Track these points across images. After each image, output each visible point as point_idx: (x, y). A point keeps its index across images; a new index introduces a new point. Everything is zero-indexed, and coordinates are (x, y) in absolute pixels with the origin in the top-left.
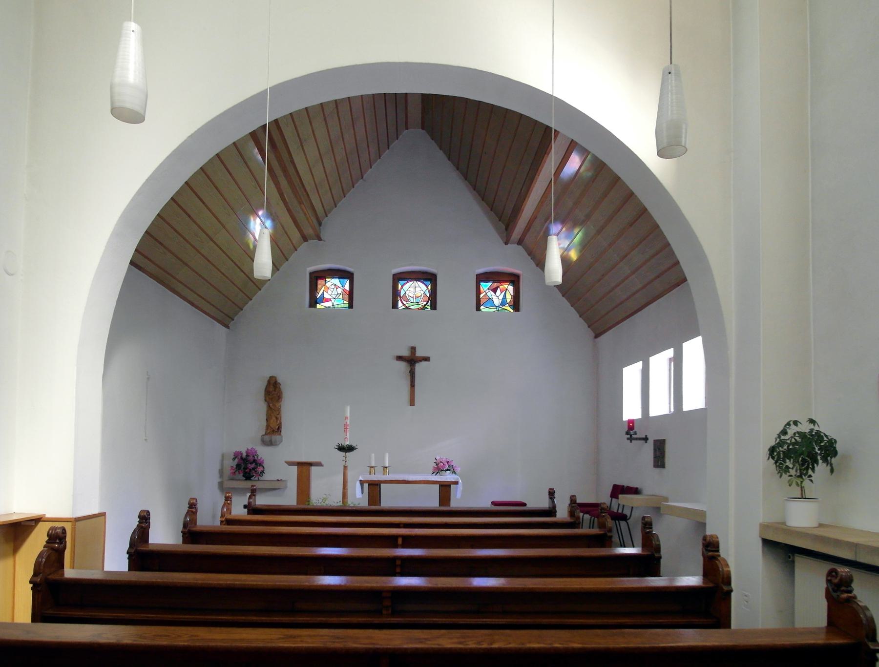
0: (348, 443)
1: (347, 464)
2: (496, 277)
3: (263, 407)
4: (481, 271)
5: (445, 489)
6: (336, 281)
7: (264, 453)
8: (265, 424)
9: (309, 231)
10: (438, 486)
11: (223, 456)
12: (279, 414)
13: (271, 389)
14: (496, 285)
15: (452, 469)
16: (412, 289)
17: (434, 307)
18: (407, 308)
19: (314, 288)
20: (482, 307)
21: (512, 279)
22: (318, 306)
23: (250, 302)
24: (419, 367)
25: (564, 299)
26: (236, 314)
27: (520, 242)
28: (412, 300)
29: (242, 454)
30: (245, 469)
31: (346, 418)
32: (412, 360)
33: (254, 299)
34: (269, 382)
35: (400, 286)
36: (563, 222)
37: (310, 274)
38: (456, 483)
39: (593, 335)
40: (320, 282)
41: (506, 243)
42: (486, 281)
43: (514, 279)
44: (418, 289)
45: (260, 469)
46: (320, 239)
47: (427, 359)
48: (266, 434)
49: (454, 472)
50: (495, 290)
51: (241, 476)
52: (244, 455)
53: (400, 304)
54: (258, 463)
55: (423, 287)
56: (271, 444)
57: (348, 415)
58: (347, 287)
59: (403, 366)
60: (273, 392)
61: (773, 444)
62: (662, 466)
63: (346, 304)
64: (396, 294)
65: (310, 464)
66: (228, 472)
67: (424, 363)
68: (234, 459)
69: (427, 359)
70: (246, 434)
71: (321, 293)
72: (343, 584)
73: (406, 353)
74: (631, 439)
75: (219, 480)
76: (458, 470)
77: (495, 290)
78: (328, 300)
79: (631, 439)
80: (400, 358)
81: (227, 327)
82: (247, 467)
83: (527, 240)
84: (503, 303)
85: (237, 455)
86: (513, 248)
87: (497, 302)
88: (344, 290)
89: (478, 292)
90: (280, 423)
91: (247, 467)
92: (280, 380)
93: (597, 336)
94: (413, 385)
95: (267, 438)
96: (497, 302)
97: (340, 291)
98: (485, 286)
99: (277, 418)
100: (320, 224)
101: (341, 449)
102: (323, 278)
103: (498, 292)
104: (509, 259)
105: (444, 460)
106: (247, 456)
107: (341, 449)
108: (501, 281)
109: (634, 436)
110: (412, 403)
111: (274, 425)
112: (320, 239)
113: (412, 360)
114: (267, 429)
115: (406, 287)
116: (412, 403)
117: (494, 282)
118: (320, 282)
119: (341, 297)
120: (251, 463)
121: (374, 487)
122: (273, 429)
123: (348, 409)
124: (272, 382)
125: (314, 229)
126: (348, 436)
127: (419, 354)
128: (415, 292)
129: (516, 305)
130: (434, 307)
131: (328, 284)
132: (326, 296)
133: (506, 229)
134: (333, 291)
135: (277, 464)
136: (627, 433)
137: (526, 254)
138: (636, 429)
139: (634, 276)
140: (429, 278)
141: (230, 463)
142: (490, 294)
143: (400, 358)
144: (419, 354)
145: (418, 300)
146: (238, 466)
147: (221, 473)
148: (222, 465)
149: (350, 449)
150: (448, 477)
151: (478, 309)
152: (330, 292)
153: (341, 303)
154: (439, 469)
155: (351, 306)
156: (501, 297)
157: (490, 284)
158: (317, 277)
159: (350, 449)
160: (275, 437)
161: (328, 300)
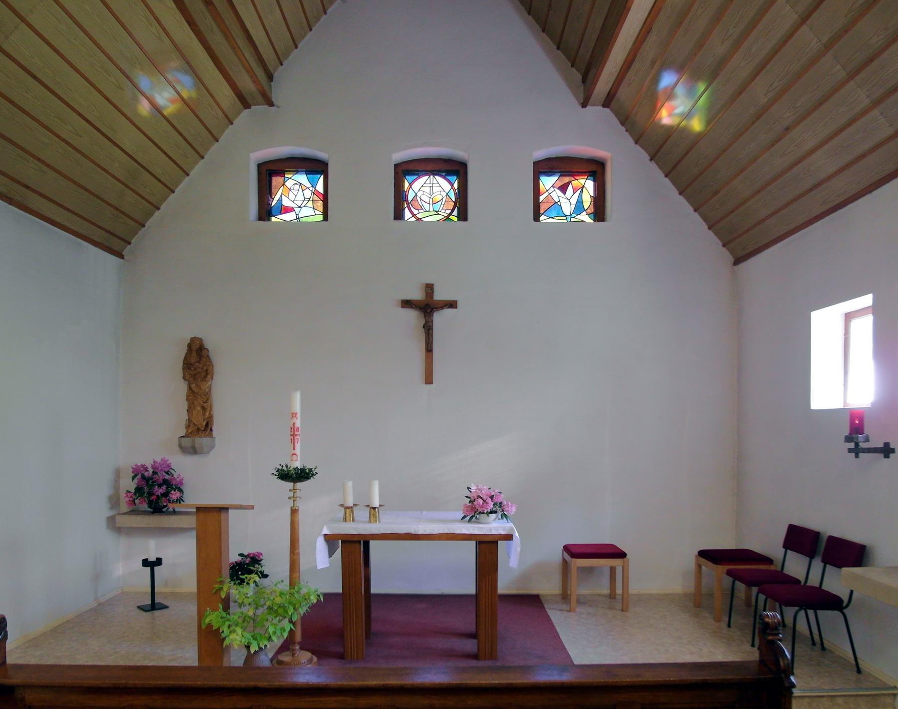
0: (298, 464)
1: (300, 505)
2: (565, 166)
3: (182, 388)
4: (541, 154)
5: (487, 549)
6: (302, 178)
7: (184, 467)
9: (246, 83)
10: (473, 543)
11: (118, 473)
13: (194, 359)
14: (566, 180)
15: (499, 509)
16: (427, 189)
17: (463, 216)
18: (418, 219)
19: (265, 190)
20: (542, 218)
21: (593, 168)
22: (273, 219)
23: (157, 213)
24: (440, 318)
25: (681, 199)
26: (135, 233)
27: (606, 104)
28: (426, 206)
29: (146, 470)
30: (149, 493)
31: (294, 415)
32: (427, 307)
33: (163, 207)
34: (189, 346)
35: (407, 184)
36: (680, 69)
37: (260, 166)
38: (509, 537)
39: (732, 260)
40: (276, 180)
41: (584, 105)
42: (549, 173)
43: (595, 169)
44: (436, 189)
45: (175, 495)
46: (271, 104)
47: (452, 305)
49: (504, 516)
50: (563, 189)
51: (145, 507)
53: (407, 214)
55: (446, 186)
56: (194, 451)
57: (297, 408)
58: (320, 187)
59: (413, 317)
60: (197, 363)
63: (321, 218)
64: (400, 200)
65: (224, 509)
67: (448, 312)
68: (133, 478)
69: (452, 305)
70: (151, 433)
71: (277, 198)
73: (417, 295)
74: (857, 451)
75: (110, 513)
76: (512, 510)
77: (563, 189)
78: (291, 210)
79: (857, 451)
80: (407, 304)
81: (121, 256)
83: (623, 93)
84: (579, 207)
85: (138, 472)
86: (596, 112)
87: (567, 209)
88: (315, 193)
89: (537, 192)
90: (211, 417)
91: (153, 494)
92: (208, 344)
93: (737, 261)
94: (429, 349)
95: (187, 442)
96: (567, 209)
97: (308, 193)
98: (547, 182)
99: (204, 408)
100: (270, 77)
101: (285, 475)
102: (281, 173)
103: (570, 190)
104: (591, 132)
105: (484, 493)
107: (285, 475)
108: (574, 174)
109: (862, 445)
110: (429, 380)
112: (271, 104)
113: (427, 307)
114: (188, 427)
115: (417, 185)
116: (429, 380)
117: (563, 174)
118: (276, 180)
119: (310, 204)
120: (160, 486)
121: (355, 551)
122: (199, 427)
123: (297, 397)
125: (256, 81)
126: (298, 451)
127: (439, 296)
128: (431, 193)
129: (599, 212)
130: (463, 216)
131: (289, 183)
132: (286, 203)
133: (584, 81)
134: (297, 194)
135: (229, 475)
136: (848, 439)
137: (615, 121)
138: (867, 430)
139: (876, 112)
140: (454, 168)
142: (556, 195)
143: (407, 304)
144: (439, 296)
145: (437, 207)
147: (114, 501)
149: (303, 475)
150: (492, 526)
151: (537, 218)
152: (292, 197)
153: (311, 213)
154: (474, 510)
155: (326, 218)
156: (574, 200)
157: (553, 179)
158: (270, 172)
159: (303, 475)
160: (202, 441)
161: (291, 210)
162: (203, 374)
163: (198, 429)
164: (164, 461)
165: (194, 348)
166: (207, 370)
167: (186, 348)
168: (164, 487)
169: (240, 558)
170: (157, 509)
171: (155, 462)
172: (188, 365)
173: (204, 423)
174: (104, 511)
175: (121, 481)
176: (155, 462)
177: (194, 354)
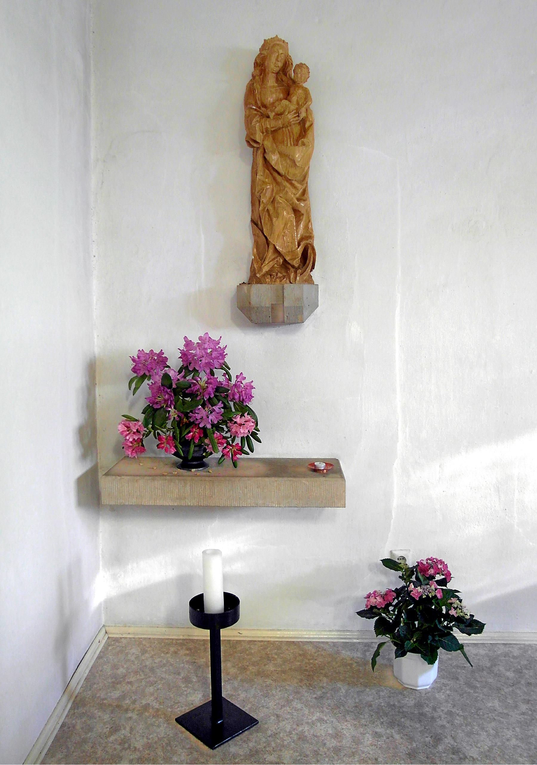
3: (234, 171)
7: (248, 354)
8: (244, 239)
11: (92, 370)
12: (304, 195)
13: (271, 93)
30: (180, 424)
34: (260, 65)
48: (254, 278)
52: (175, 362)
54: (233, 400)
60: (276, 107)
61: (77, 470)
62: (332, 468)
66: (111, 432)
70: (170, 282)
72: (93, 465)
82: (184, 424)
85: (146, 365)
90: (308, 236)
95: (262, 294)
99: (296, 211)
106: (185, 369)
111: (285, 240)
122: (280, 267)
124: (274, 65)
141: (124, 402)
146: (153, 413)
147: (88, 437)
148: (90, 406)
160: (292, 290)
162: (296, 129)
163: (286, 265)
164: (205, 340)
165: (274, 65)
166: (303, 122)
167: (250, 68)
168: (218, 407)
169: (392, 581)
170: (191, 459)
171: (188, 343)
172: (255, 104)
173: (300, 250)
174: (66, 466)
175: (98, 391)
176: (188, 343)
177: (271, 81)
